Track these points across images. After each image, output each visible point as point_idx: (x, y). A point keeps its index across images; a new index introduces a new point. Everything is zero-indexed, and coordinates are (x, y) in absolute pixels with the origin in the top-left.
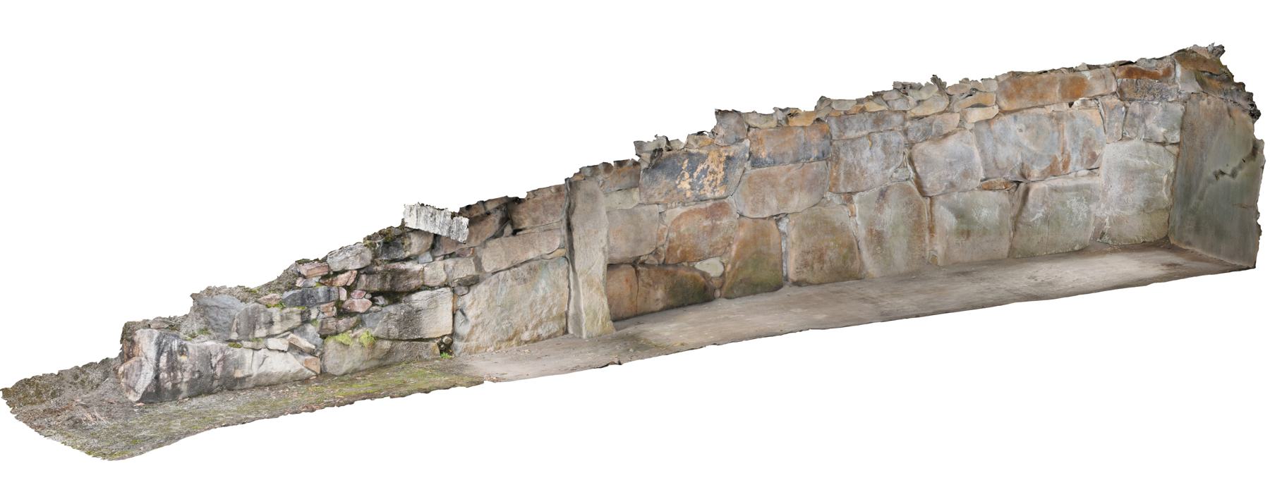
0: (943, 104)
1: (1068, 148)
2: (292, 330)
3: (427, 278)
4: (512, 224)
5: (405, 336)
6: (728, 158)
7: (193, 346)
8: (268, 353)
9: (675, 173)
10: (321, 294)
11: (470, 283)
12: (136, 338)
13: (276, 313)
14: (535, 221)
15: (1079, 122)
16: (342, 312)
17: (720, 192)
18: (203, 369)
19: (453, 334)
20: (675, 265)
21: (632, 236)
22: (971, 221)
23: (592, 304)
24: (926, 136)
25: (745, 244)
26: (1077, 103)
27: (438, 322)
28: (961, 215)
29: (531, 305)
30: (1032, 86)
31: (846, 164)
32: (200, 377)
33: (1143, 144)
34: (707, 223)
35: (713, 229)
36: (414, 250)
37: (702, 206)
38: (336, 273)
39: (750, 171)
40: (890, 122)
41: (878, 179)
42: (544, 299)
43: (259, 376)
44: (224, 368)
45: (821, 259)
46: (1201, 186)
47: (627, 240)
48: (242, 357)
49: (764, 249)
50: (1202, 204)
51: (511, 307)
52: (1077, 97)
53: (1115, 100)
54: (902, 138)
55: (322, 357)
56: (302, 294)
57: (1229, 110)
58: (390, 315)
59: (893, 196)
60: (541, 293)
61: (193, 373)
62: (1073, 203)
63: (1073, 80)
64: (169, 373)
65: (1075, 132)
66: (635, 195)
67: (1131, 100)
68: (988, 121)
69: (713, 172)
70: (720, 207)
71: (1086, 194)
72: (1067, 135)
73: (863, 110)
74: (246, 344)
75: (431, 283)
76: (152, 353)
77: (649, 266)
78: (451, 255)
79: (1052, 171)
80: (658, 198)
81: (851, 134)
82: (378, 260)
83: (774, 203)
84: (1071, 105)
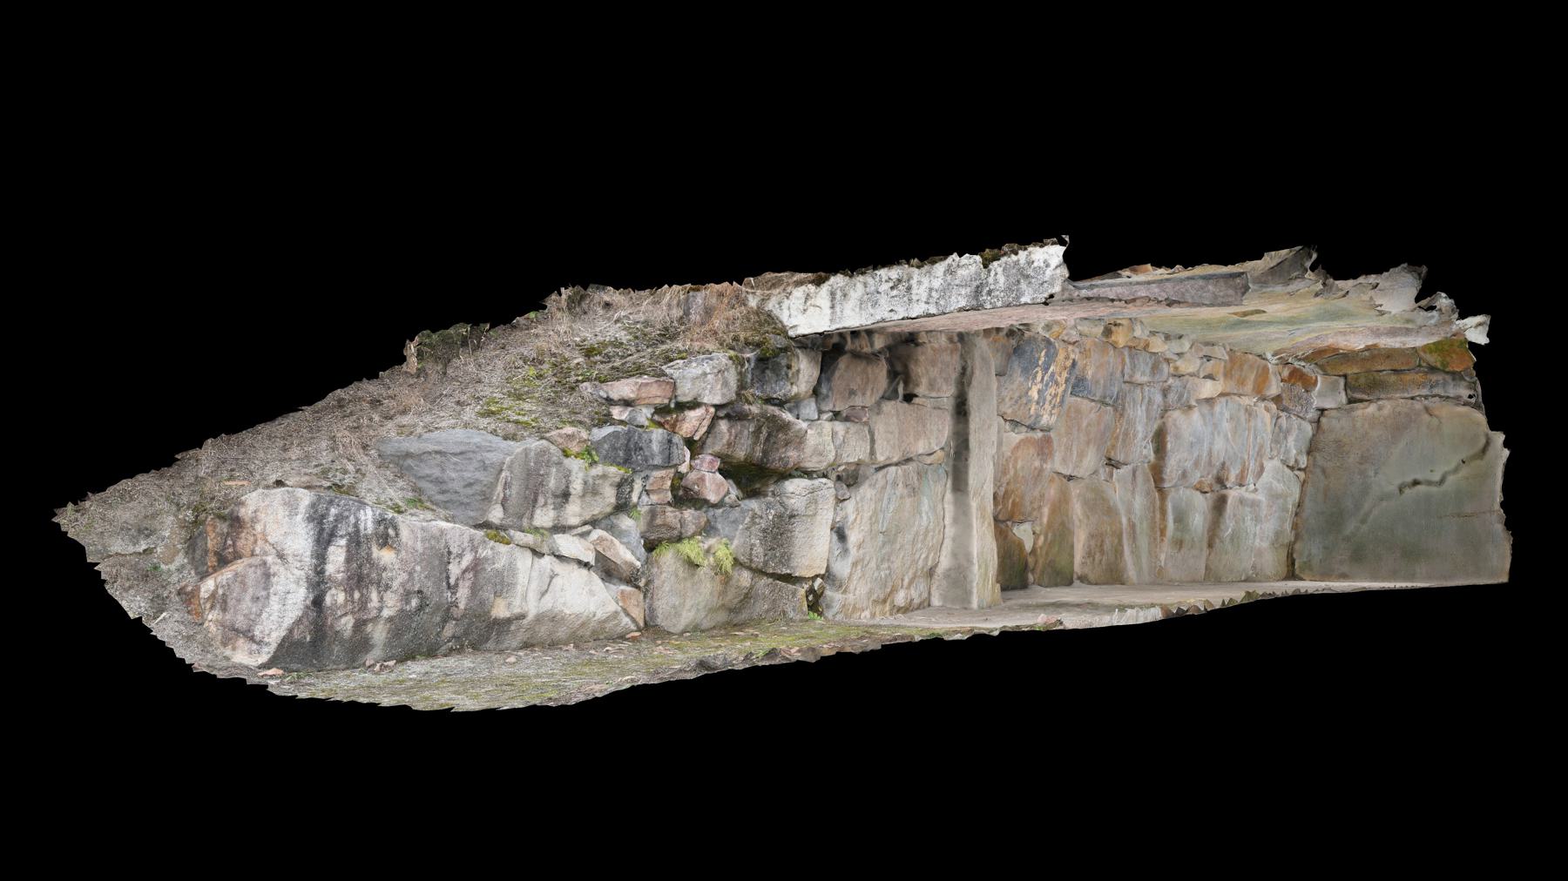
2: (594, 523)
3: (808, 451)
4: (906, 383)
7: (412, 527)
8: (559, 568)
10: (655, 447)
12: (245, 513)
18: (429, 588)
32: (420, 608)
38: (682, 407)
43: (539, 619)
44: (475, 590)
46: (1366, 506)
48: (512, 568)
50: (1365, 528)
55: (646, 592)
57: (1427, 409)
61: (407, 596)
64: (349, 591)
74: (519, 536)
75: (810, 465)
76: (300, 541)
82: (748, 393)
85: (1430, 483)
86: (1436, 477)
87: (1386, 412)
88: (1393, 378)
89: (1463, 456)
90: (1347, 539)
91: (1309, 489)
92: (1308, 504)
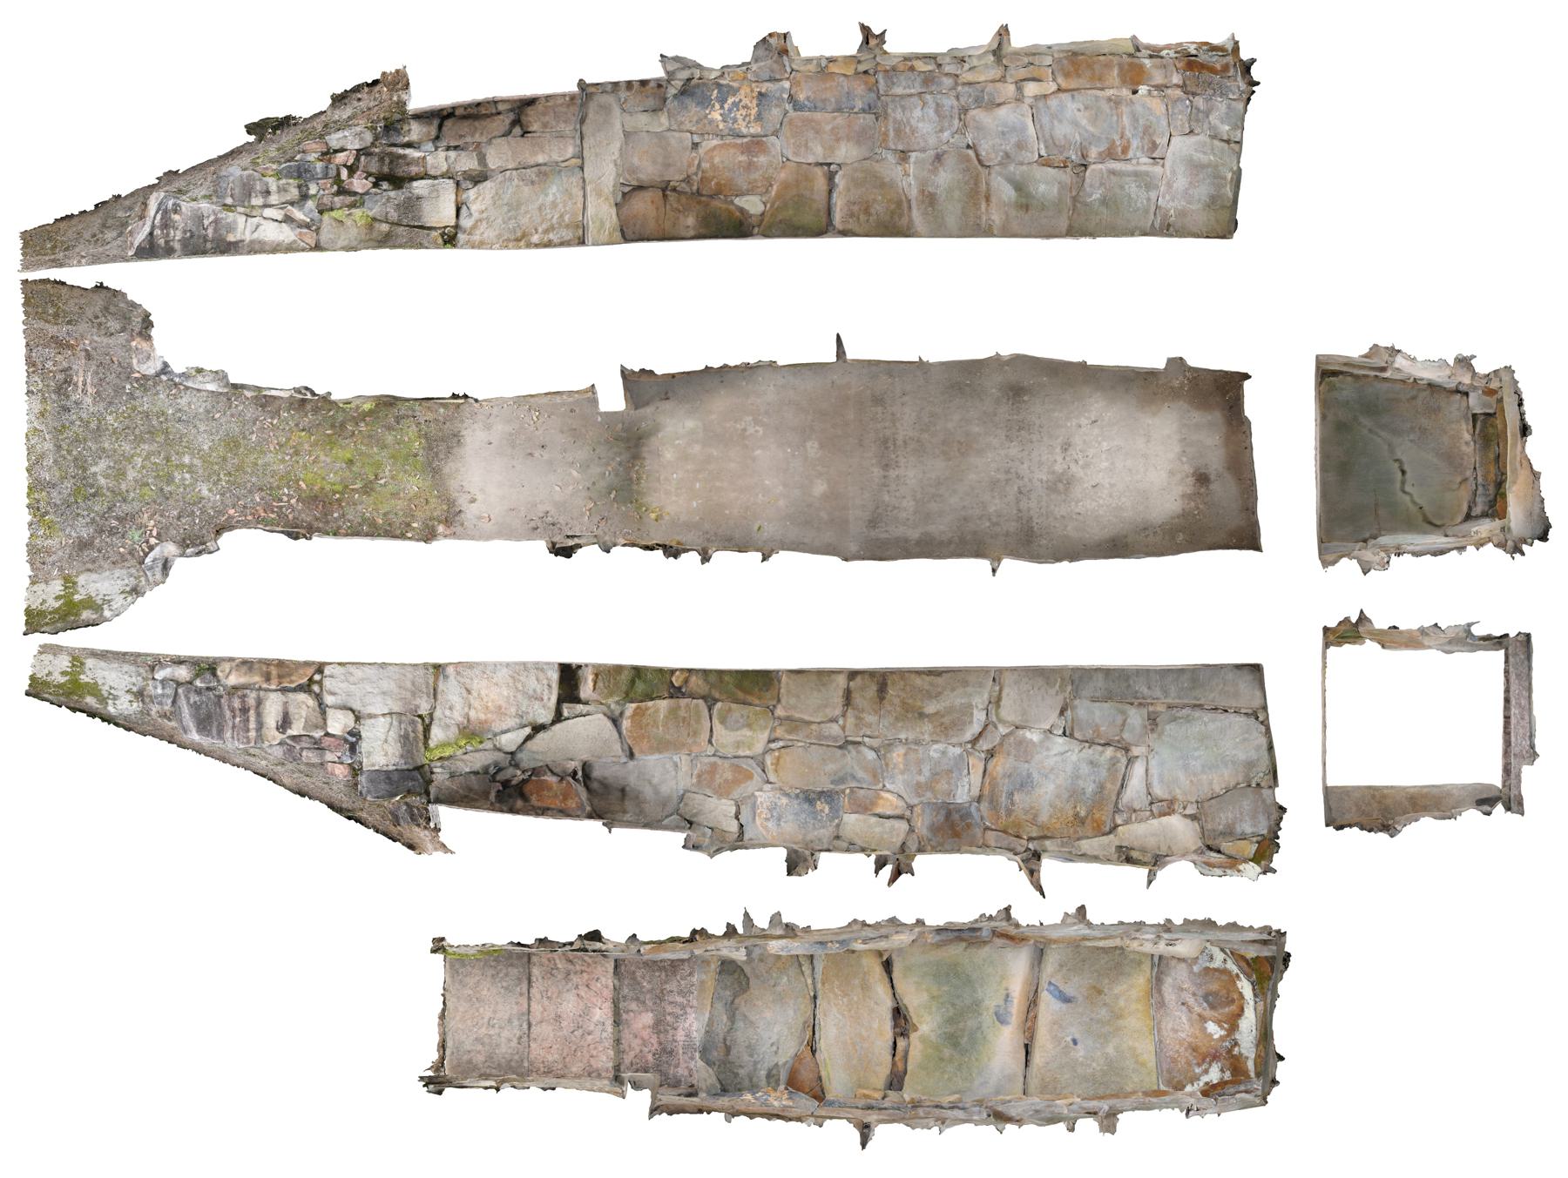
0: (995, 73)
1: (1128, 134)
5: (405, 222)
6: (760, 94)
7: (185, 207)
9: (705, 102)
11: (478, 178)
13: (273, 185)
14: (545, 125)
15: (1139, 108)
16: (342, 191)
17: (755, 129)
19: (457, 227)
20: (711, 196)
21: (660, 160)
22: (1028, 195)
23: (602, 211)
24: (979, 102)
25: (786, 186)
26: (1143, 89)
27: (441, 212)
28: (1019, 187)
29: (540, 209)
30: (1090, 66)
31: (895, 121)
33: (1208, 140)
34: (743, 158)
35: (750, 166)
36: (414, 137)
37: (739, 141)
38: (336, 151)
39: (792, 113)
40: (940, 84)
41: (932, 141)
42: (554, 205)
43: (252, 242)
44: (216, 230)
45: (867, 211)
46: (1383, 433)
47: (654, 162)
48: (235, 222)
49: (807, 193)
51: (519, 205)
52: (1139, 83)
53: (1178, 92)
54: (955, 103)
55: (317, 231)
56: (299, 167)
58: (389, 199)
59: (950, 161)
60: (551, 198)
62: (1132, 188)
63: (1131, 65)
65: (1135, 118)
66: (664, 119)
67: (1194, 94)
68: (1045, 96)
69: (745, 107)
70: (756, 145)
71: (1147, 182)
72: (1126, 120)
73: (912, 69)
75: (432, 172)
77: (680, 193)
78: (456, 148)
79: (1110, 154)
80: (688, 126)
81: (899, 90)
83: (819, 150)
84: (1135, 92)
85: (1403, 483)
86: (1407, 489)
87: (1464, 448)
88: (1492, 456)
89: (1426, 508)
90: (1355, 419)
91: (1398, 386)
92: (1386, 385)
